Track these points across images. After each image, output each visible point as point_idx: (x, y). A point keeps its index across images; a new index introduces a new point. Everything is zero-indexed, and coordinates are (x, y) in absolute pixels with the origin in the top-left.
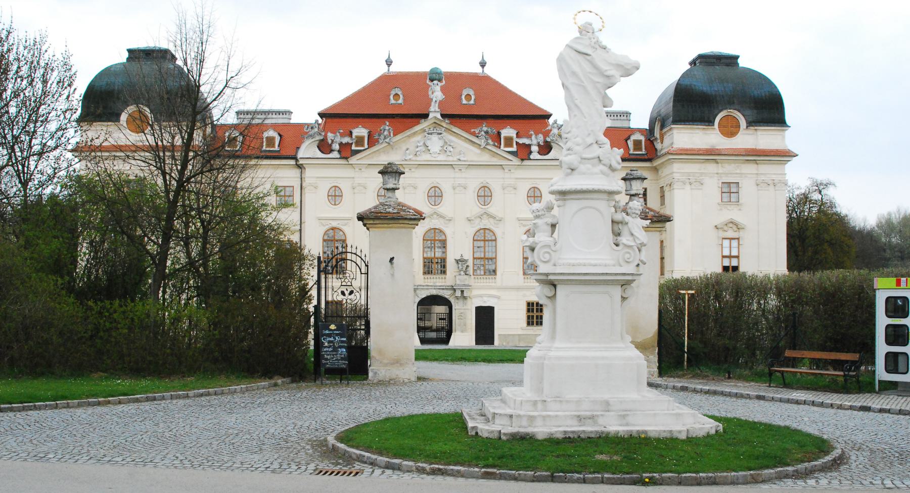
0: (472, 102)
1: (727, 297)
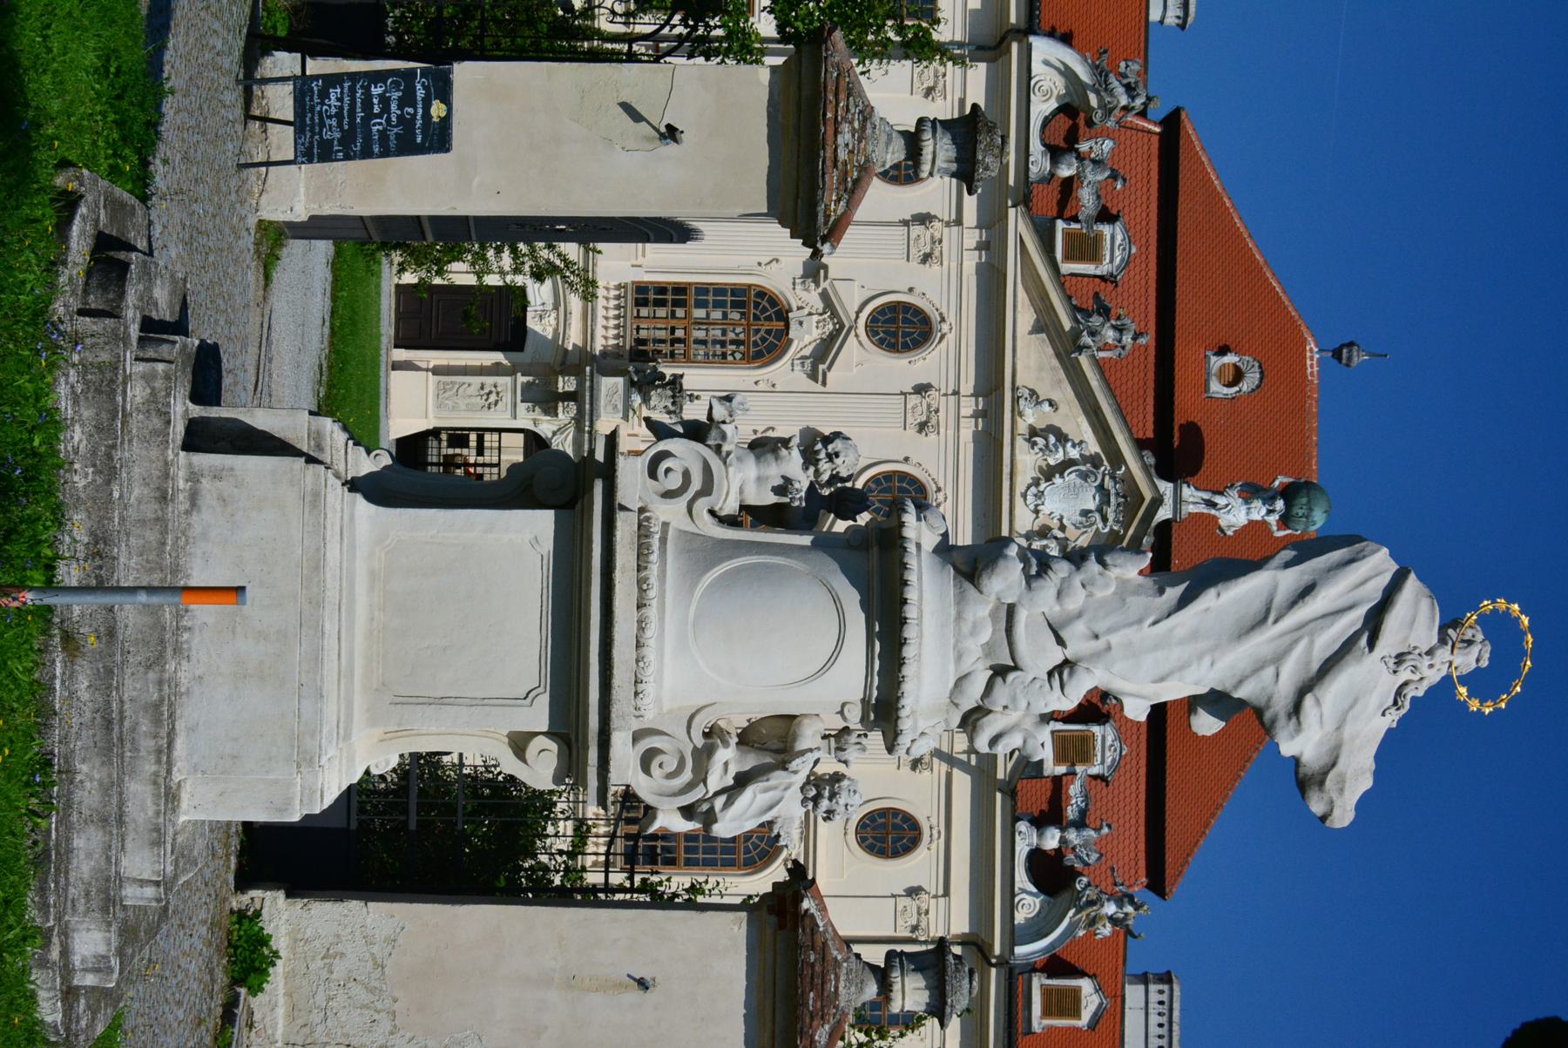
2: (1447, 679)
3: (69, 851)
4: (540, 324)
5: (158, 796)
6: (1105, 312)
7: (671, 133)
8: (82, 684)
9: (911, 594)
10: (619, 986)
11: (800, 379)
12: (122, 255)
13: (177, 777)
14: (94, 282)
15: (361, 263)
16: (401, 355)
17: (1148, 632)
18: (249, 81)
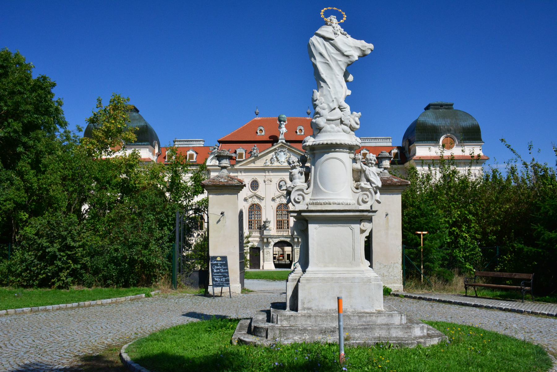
0: (303, 133)
1: (448, 257)
2: (339, 24)
3: (396, 337)
4: (256, 244)
5: (381, 316)
6: (251, 152)
7: (222, 213)
8: (357, 335)
9: (325, 142)
10: (387, 219)
11: (263, 202)
12: (253, 328)
13: (374, 311)
14: (259, 335)
15: (247, 274)
16: (261, 268)
17: (332, 89)
18: (214, 296)
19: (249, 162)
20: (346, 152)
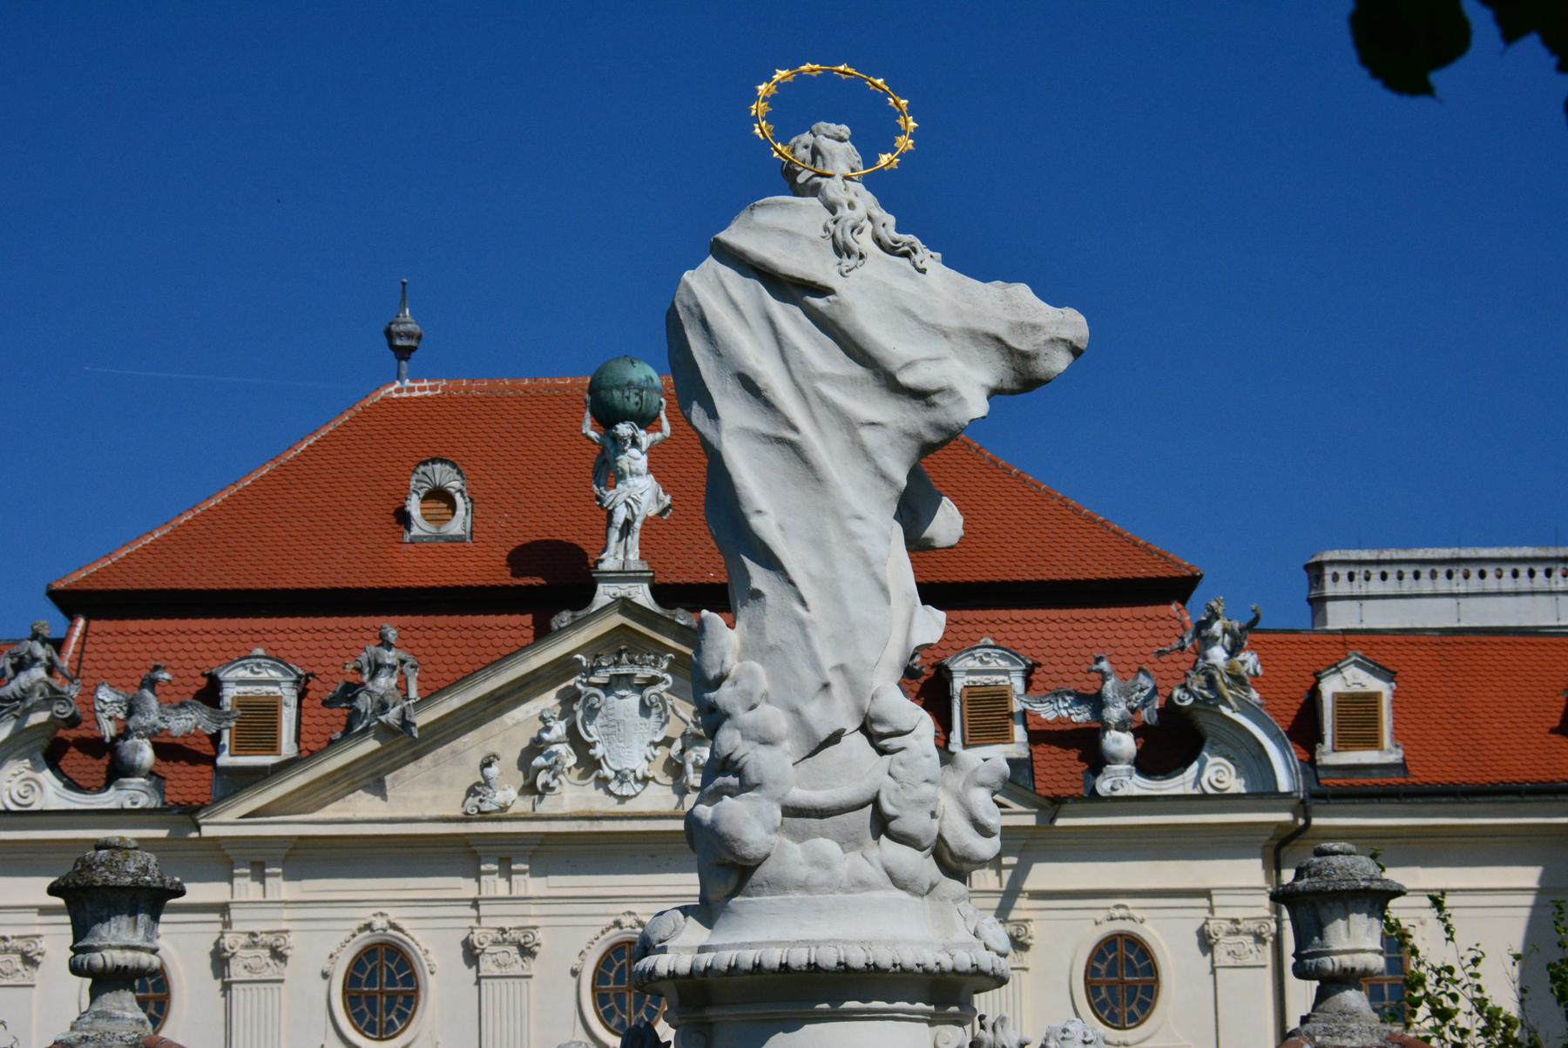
6: (351, 691)
9: (773, 958)
17: (817, 613)
19: (331, 779)
20: (909, 1017)
